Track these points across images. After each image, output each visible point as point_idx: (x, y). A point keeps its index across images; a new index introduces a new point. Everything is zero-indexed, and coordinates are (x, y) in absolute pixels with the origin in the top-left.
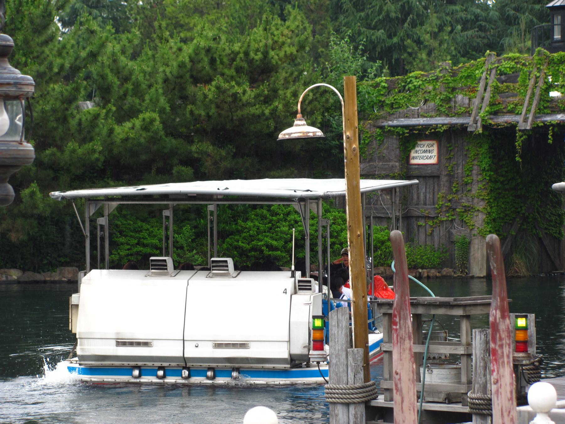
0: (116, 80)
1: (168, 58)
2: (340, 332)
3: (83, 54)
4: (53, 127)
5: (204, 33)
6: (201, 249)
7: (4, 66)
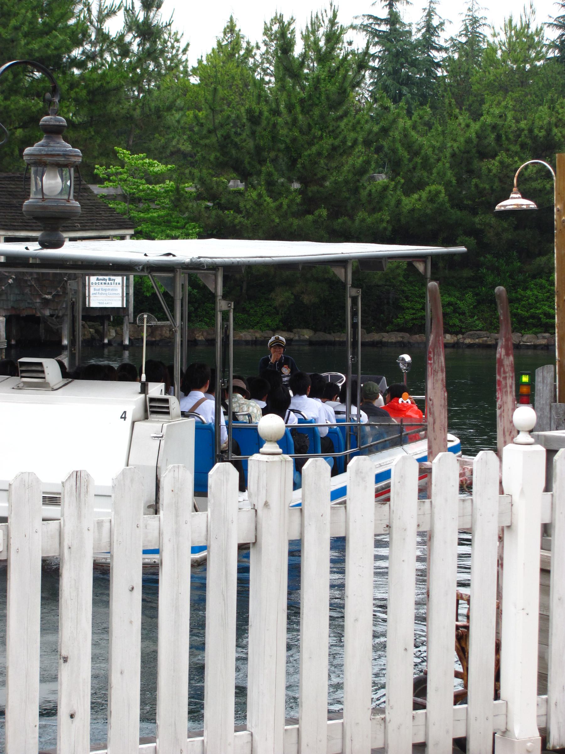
0: (406, 154)
1: (457, 134)
2: (545, 388)
3: (376, 129)
4: (345, 197)
5: (491, 110)
6: (482, 315)
7: (58, 141)
